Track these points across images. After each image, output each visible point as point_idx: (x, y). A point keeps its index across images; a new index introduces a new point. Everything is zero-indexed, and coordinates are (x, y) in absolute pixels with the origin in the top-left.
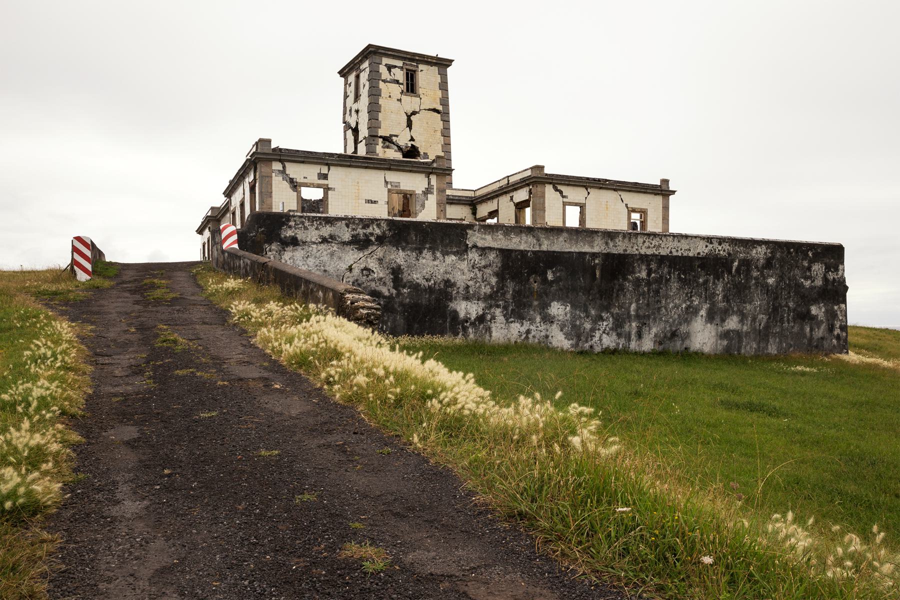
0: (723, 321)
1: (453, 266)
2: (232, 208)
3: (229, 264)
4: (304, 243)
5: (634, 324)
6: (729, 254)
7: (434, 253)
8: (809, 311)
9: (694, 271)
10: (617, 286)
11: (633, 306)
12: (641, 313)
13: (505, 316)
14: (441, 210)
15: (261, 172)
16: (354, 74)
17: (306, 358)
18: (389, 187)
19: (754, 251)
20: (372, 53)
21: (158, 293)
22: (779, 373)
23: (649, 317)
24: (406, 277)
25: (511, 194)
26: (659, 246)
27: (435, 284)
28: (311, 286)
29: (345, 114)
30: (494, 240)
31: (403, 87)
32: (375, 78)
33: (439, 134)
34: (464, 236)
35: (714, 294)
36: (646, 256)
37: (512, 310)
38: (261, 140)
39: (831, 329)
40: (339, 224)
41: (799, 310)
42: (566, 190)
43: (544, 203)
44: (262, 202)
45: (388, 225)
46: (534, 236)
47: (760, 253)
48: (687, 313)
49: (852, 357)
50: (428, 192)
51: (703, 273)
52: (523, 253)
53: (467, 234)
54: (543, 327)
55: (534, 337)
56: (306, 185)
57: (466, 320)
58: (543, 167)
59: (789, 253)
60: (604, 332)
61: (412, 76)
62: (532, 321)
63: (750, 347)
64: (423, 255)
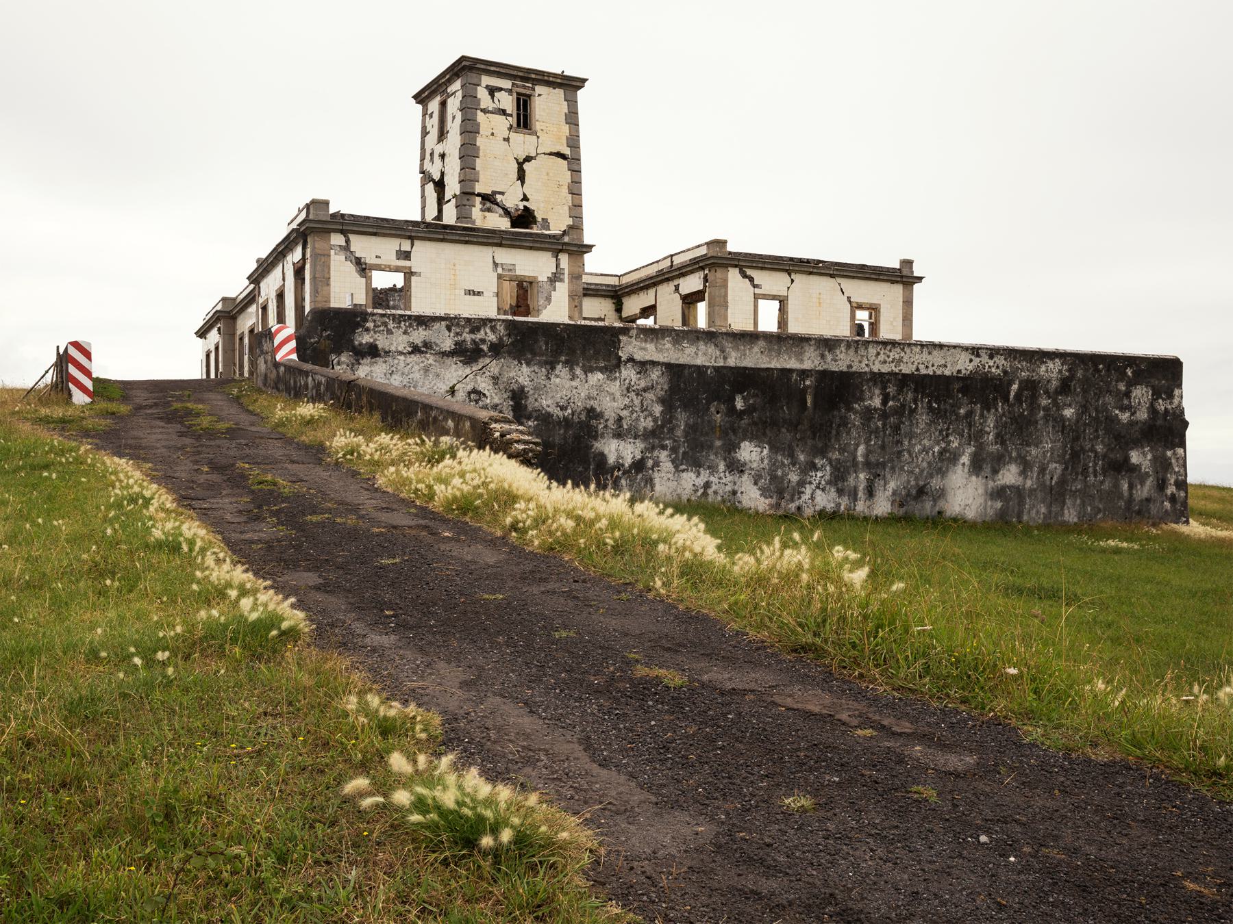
0: (995, 472)
1: (600, 389)
2: (261, 301)
3: (286, 383)
4: (387, 353)
5: (862, 476)
6: (1005, 372)
7: (571, 369)
8: (1127, 459)
9: (952, 398)
10: (838, 420)
11: (861, 449)
12: (872, 459)
13: (673, 462)
14: (575, 306)
15: (313, 249)
16: (438, 99)
17: (472, 503)
18: (500, 270)
19: (1043, 368)
20: (466, 68)
21: (205, 422)
22: (1081, 550)
23: (884, 465)
24: (531, 404)
25: (676, 282)
26: (901, 360)
27: (573, 414)
28: (434, 413)
29: (422, 159)
30: (659, 350)
31: (513, 120)
32: (469, 106)
33: (565, 190)
34: (616, 344)
35: (982, 432)
36: (881, 374)
37: (684, 453)
38: (314, 202)
39: (1161, 485)
40: (437, 326)
41: (1112, 456)
42: (759, 276)
43: (726, 295)
44: (315, 292)
45: (506, 328)
46: (716, 345)
47: (1051, 371)
48: (941, 460)
49: (1195, 528)
50: (555, 278)
51: (965, 400)
52: (700, 370)
53: (619, 341)
54: (729, 478)
55: (715, 493)
56: (379, 268)
57: (618, 466)
58: (724, 243)
59: (1097, 370)
60: (818, 487)
61: (525, 103)
62: (713, 469)
63: (1036, 512)
64: (557, 372)
